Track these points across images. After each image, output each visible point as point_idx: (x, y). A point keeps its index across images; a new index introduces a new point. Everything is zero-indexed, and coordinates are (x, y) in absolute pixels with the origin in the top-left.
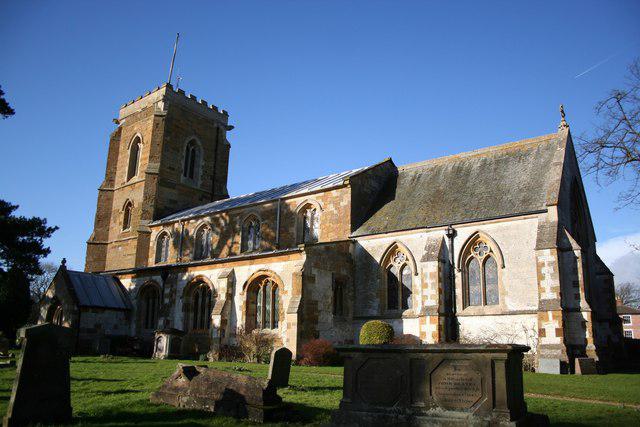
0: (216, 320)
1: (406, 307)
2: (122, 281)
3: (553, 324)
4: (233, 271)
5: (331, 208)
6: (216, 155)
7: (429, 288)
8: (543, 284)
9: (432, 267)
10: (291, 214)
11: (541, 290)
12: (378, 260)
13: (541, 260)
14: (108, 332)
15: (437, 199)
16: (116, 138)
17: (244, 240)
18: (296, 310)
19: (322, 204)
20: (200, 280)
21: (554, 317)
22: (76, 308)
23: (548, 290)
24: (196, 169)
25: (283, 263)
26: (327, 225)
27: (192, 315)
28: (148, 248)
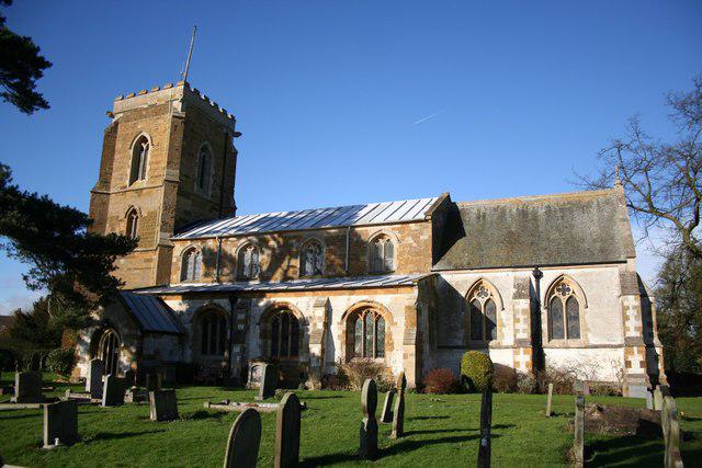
0: (316, 349)
1: (490, 338)
2: (167, 302)
3: (637, 358)
4: (328, 301)
5: (410, 240)
6: (225, 162)
7: (522, 322)
8: (628, 324)
9: (525, 304)
10: (363, 243)
11: (626, 329)
12: (463, 294)
13: (626, 304)
14: (166, 358)
15: (511, 240)
16: (111, 133)
17: (302, 264)
18: (414, 341)
19: (399, 236)
20: (285, 307)
21: (639, 352)
22: (139, 333)
23: (632, 329)
24: (206, 178)
25: (391, 296)
26: (405, 256)
27: (269, 342)
28: (170, 264)
